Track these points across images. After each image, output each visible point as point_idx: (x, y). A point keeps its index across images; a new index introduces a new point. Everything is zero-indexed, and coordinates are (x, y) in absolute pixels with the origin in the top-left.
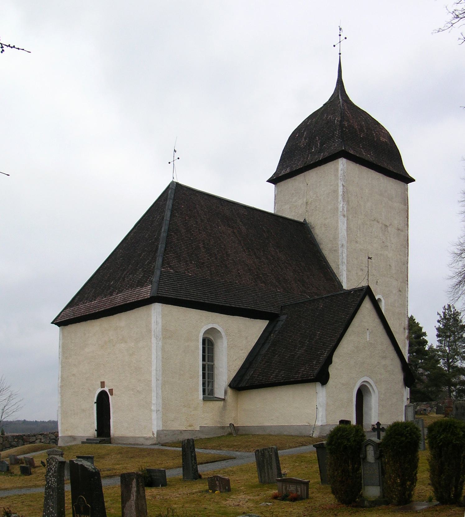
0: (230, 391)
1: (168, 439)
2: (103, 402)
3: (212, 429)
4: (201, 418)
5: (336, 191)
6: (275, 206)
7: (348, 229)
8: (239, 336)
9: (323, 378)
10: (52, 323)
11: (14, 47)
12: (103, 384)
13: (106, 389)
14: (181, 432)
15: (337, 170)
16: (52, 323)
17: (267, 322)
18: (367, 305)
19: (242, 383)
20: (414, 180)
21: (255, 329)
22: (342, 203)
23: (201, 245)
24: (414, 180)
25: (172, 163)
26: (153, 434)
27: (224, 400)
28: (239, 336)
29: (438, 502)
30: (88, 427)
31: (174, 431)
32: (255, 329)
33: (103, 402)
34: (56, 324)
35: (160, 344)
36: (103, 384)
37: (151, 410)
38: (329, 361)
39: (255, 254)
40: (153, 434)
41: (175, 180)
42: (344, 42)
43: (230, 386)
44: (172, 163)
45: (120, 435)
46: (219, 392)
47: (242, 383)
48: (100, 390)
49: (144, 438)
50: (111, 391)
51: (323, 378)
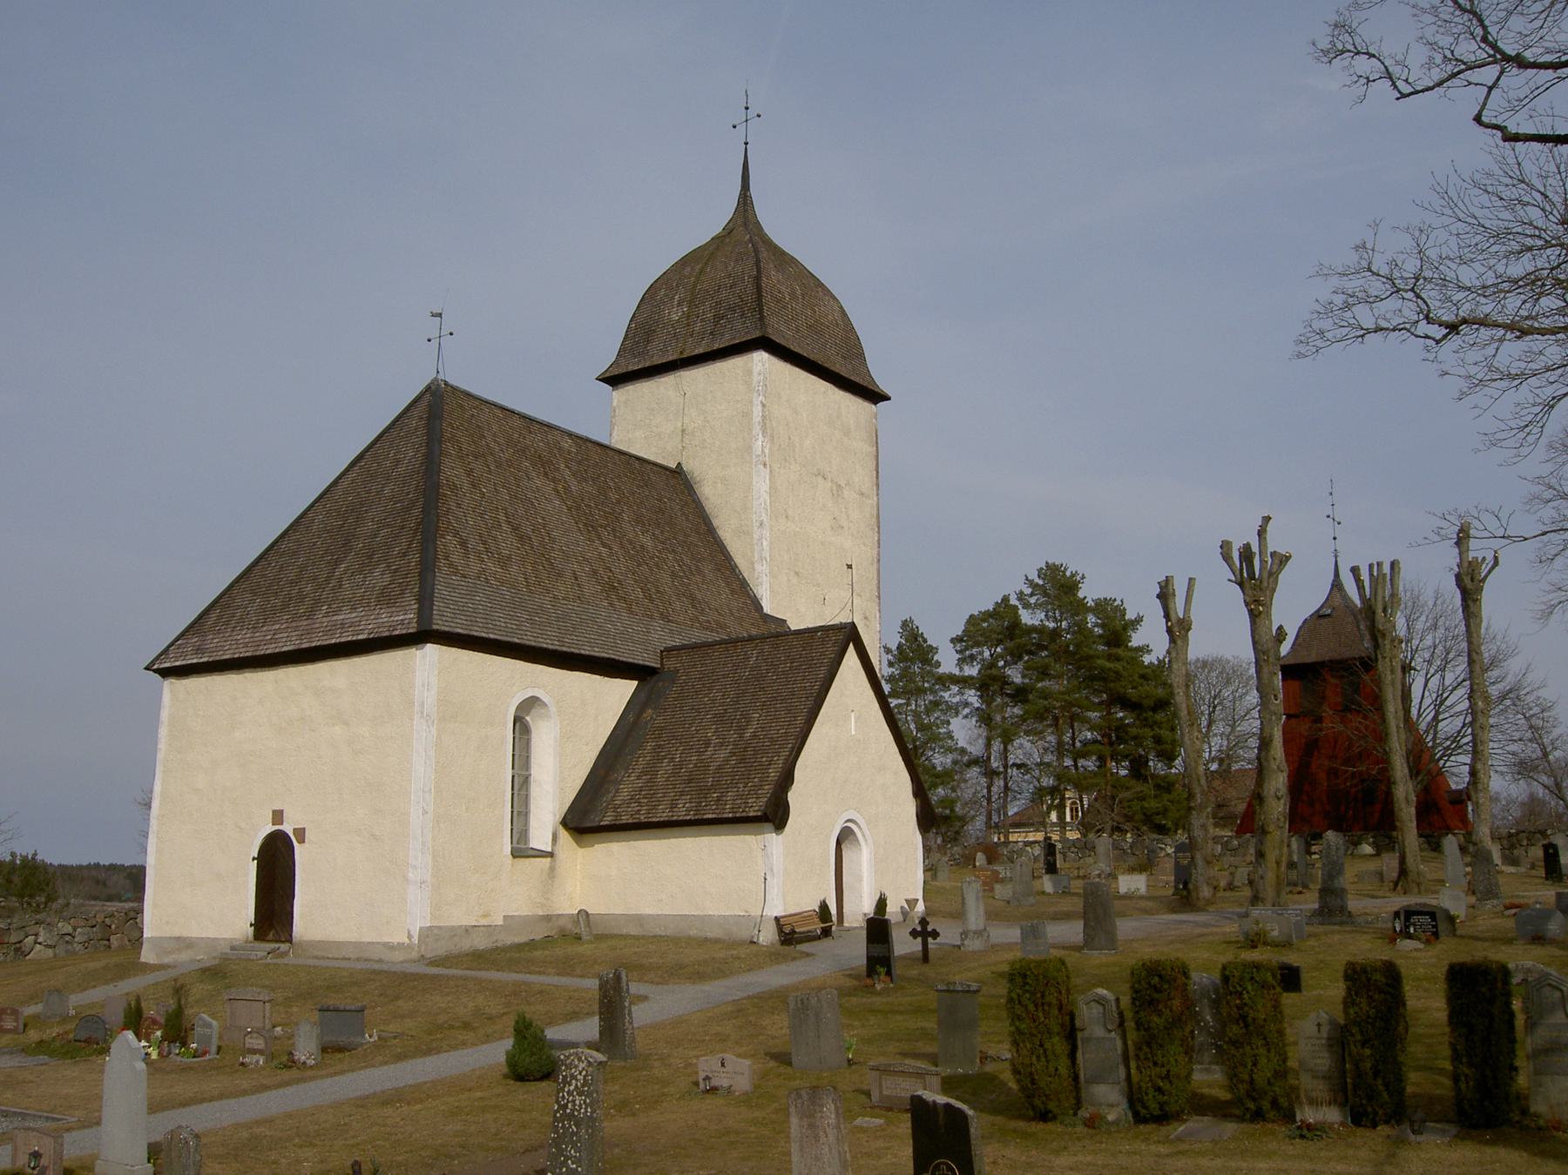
0: (564, 835)
1: (441, 948)
2: (276, 863)
3: (527, 921)
4: (504, 899)
5: (747, 415)
6: (571, 435)
7: (773, 489)
8: (584, 713)
9: (775, 815)
10: (147, 668)
11: (1484, 39)
12: (278, 816)
13: (287, 828)
14: (468, 930)
15: (749, 372)
16: (147, 668)
17: (635, 683)
18: (851, 657)
19: (586, 820)
20: (887, 398)
21: (613, 696)
22: (761, 438)
23: (502, 518)
24: (887, 398)
25: (435, 343)
26: (410, 936)
27: (551, 855)
28: (584, 713)
29: (552, 1034)
30: (229, 913)
31: (452, 928)
32: (613, 696)
33: (276, 863)
34: (155, 671)
35: (434, 732)
36: (278, 816)
37: (406, 880)
38: (787, 779)
39: (599, 538)
40: (410, 936)
41: (441, 376)
42: (753, 123)
43: (565, 823)
44: (435, 343)
45: (318, 938)
46: (540, 838)
47: (586, 820)
48: (270, 828)
49: (385, 945)
50: (301, 834)
51: (775, 815)
